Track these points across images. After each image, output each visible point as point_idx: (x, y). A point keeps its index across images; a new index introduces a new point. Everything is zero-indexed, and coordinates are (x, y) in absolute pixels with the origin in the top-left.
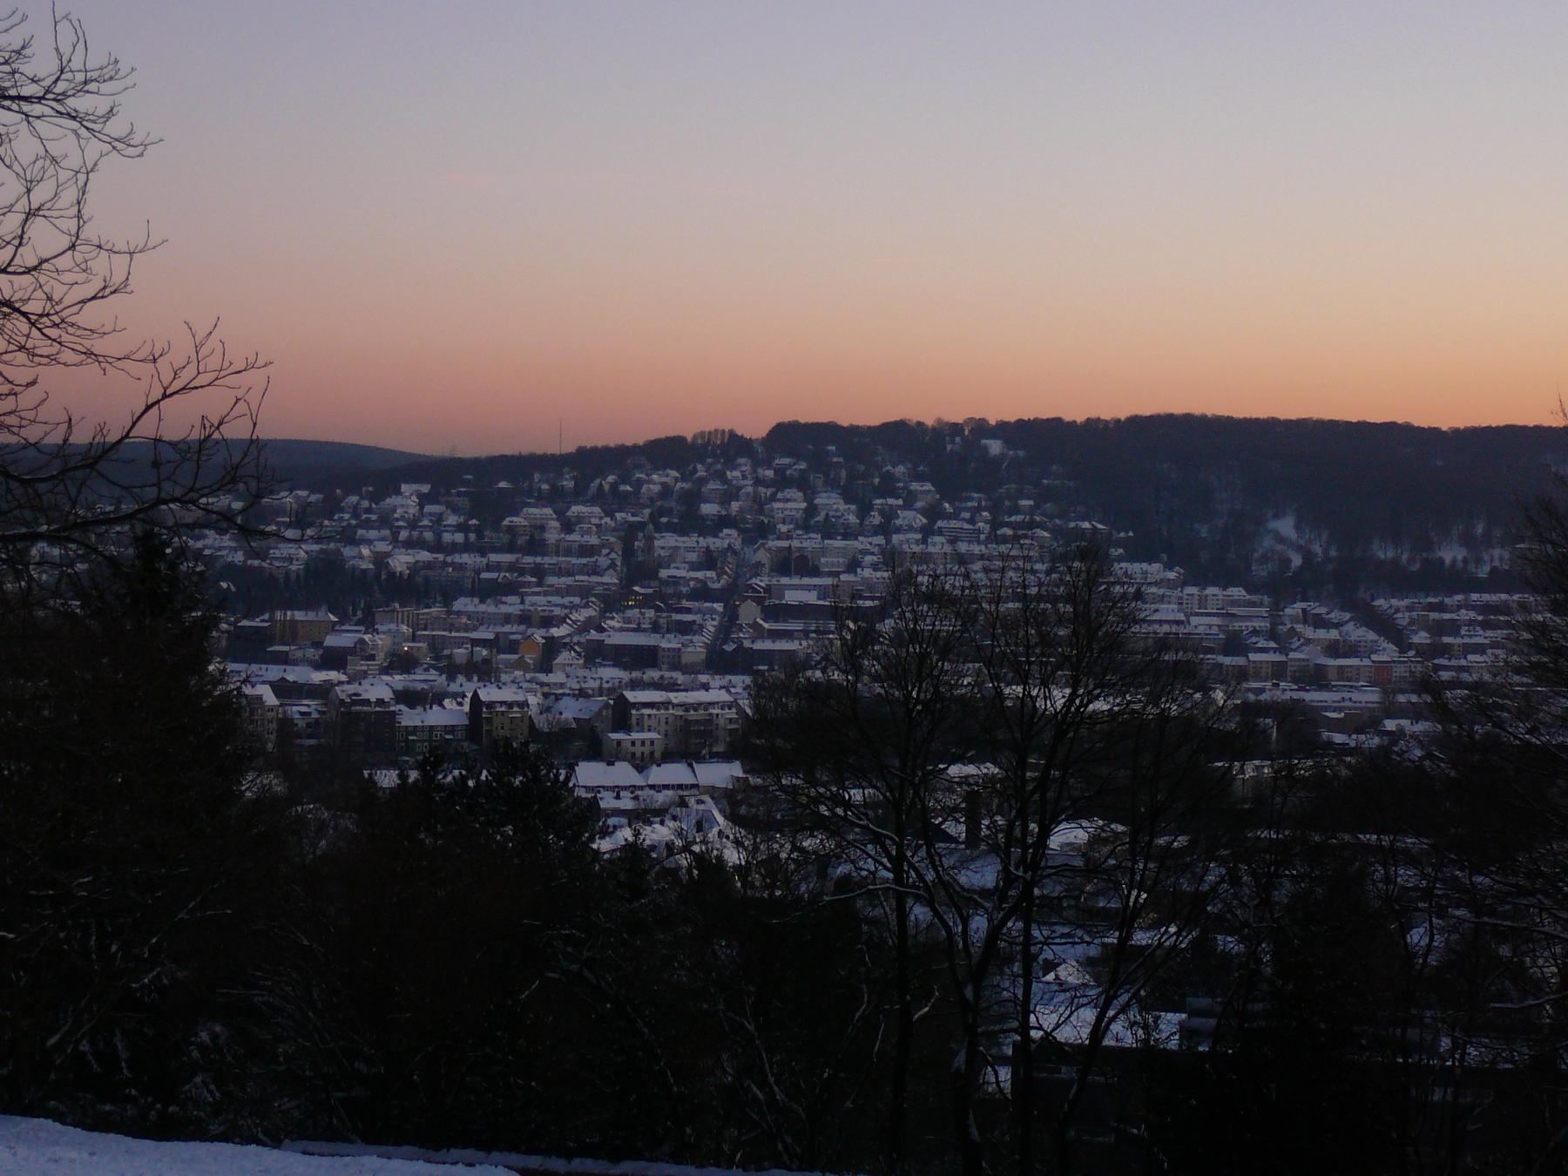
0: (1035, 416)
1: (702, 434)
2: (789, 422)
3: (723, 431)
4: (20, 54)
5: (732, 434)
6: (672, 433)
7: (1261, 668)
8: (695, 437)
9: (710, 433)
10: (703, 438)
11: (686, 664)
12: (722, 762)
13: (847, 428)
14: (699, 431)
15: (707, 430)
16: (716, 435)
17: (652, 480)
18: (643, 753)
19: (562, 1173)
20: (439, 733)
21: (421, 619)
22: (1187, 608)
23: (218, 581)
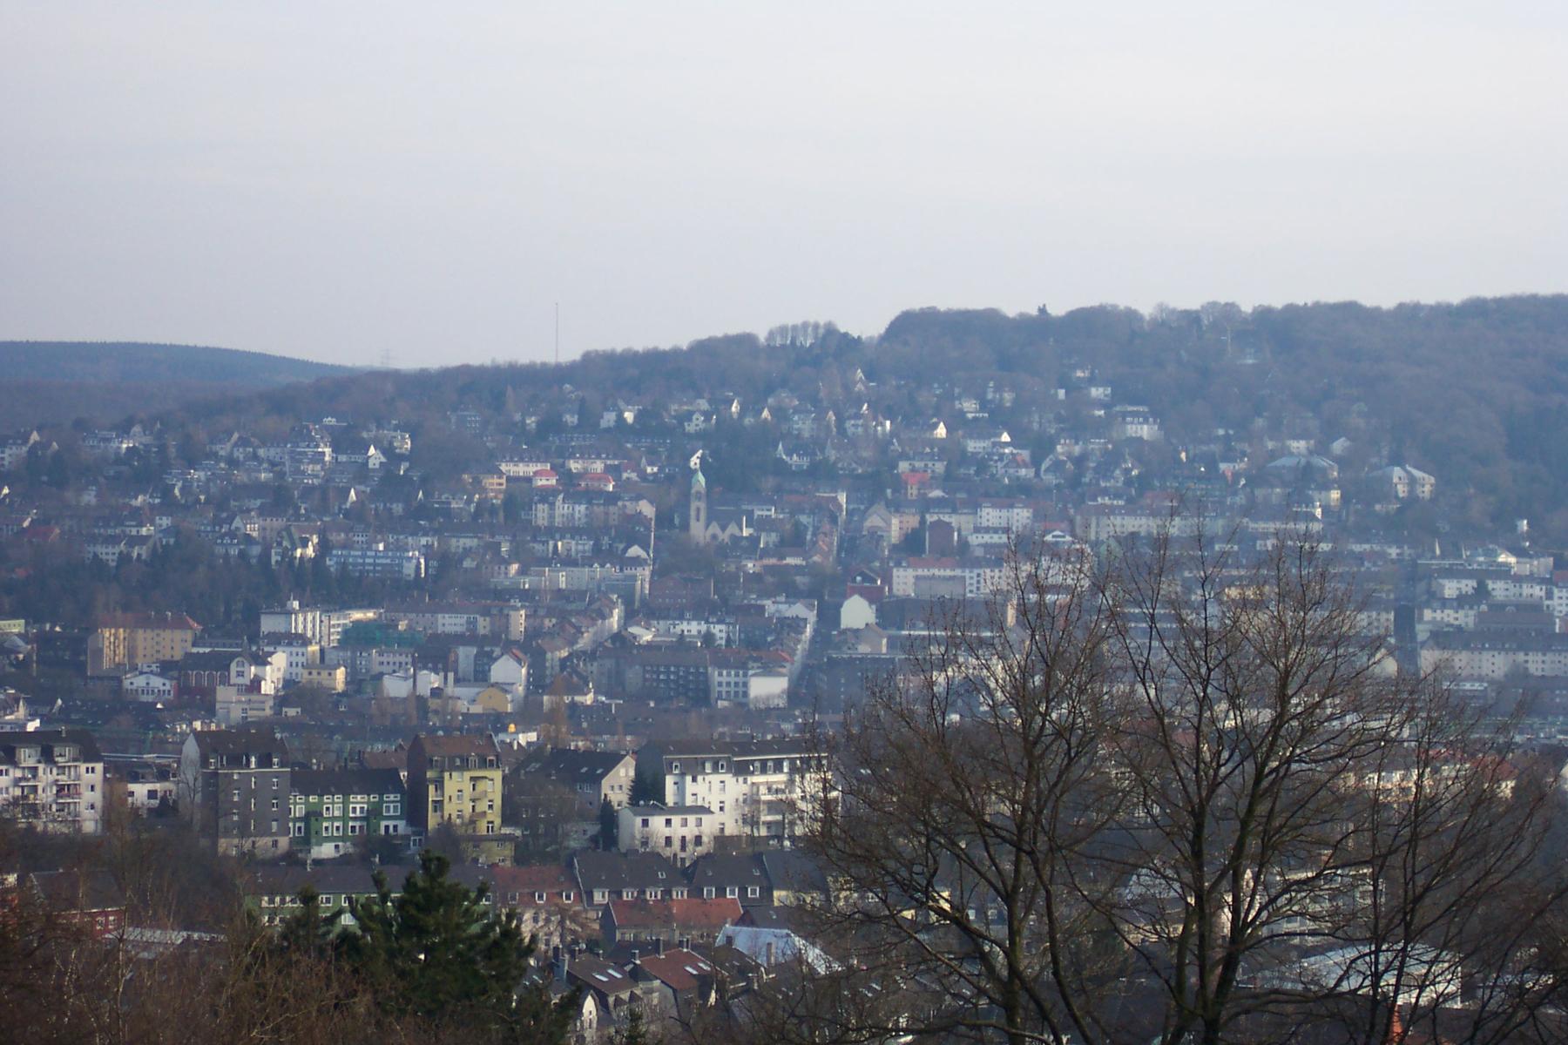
0: (1315, 299)
1: (783, 330)
2: (922, 309)
3: (816, 326)
4: (1092, 700)
5: (831, 331)
6: (734, 329)
7: (1527, 662)
8: (771, 335)
9: (795, 328)
10: (784, 336)
11: (756, 697)
12: (768, 698)
13: (1014, 320)
14: (778, 325)
15: (790, 324)
16: (806, 331)
17: (260, 557)
18: (684, 838)
19: (685, 348)
20: (358, 806)
21: (334, 626)
22: (1561, 605)
23: (631, 426)
